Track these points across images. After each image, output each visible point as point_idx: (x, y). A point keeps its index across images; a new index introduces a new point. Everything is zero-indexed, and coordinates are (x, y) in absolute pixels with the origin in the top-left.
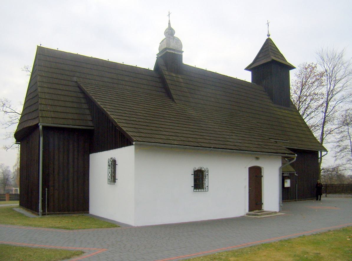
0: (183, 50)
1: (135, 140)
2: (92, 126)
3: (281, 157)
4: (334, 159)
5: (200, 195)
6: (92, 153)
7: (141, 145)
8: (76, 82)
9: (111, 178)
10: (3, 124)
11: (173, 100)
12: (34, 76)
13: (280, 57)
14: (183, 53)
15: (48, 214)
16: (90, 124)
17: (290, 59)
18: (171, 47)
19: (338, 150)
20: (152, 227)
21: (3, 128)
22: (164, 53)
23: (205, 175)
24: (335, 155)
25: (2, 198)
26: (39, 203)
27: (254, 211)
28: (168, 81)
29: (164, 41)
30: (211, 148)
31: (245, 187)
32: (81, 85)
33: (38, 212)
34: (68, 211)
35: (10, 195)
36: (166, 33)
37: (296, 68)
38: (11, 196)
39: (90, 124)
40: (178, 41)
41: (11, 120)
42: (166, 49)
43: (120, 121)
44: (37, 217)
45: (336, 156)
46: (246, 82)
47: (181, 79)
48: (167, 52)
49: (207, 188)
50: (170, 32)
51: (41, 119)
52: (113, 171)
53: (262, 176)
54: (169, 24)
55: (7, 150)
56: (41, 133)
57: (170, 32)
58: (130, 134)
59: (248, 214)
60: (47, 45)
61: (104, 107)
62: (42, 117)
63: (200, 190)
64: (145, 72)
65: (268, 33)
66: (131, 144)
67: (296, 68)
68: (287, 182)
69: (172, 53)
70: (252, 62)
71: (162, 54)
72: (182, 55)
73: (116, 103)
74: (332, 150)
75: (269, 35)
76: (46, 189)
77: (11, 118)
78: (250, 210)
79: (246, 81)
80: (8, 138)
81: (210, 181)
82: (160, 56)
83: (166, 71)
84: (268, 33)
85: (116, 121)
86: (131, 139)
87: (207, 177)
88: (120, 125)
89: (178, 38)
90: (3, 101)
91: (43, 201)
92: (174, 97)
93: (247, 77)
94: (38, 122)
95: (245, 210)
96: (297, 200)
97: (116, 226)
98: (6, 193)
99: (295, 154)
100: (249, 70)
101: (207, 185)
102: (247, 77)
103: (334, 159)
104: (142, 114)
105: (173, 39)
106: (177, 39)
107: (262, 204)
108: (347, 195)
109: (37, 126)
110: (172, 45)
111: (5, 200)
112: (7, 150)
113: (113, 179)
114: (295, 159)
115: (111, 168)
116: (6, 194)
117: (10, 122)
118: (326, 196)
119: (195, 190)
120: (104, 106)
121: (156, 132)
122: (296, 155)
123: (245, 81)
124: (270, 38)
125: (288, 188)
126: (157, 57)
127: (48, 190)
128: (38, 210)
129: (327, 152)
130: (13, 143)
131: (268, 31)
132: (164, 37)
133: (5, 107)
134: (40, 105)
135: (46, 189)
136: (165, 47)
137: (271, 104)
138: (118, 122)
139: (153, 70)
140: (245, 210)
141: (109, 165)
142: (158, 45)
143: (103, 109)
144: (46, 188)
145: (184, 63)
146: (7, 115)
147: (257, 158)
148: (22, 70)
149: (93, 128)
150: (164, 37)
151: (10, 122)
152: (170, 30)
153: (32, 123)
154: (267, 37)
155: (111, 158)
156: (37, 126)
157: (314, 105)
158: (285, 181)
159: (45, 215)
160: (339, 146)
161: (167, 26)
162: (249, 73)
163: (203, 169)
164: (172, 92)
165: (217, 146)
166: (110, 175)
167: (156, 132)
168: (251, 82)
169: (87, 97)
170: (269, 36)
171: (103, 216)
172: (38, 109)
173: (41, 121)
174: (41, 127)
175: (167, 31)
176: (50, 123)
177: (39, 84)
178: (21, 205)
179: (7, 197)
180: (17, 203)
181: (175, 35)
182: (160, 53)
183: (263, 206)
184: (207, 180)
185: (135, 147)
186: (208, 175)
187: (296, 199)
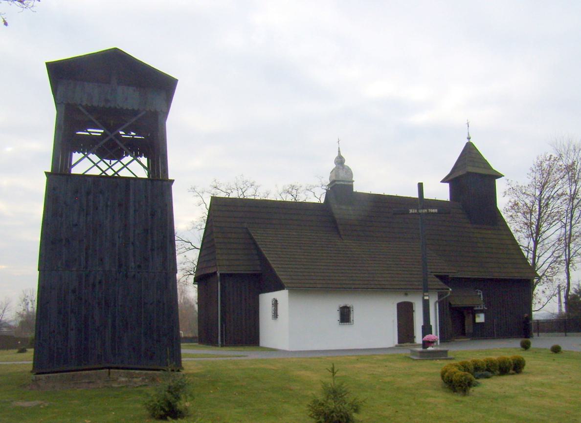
5: (346, 327)
6: (261, 293)
8: (247, 228)
16: (259, 268)
17: (496, 165)
18: (340, 178)
29: (334, 171)
31: (393, 321)
33: (218, 343)
34: (246, 343)
36: (336, 162)
37: (503, 176)
40: (349, 172)
46: (438, 200)
48: (336, 184)
50: (340, 161)
51: (218, 267)
54: (339, 151)
56: (219, 279)
57: (340, 161)
59: (396, 346)
63: (345, 323)
65: (469, 135)
67: (503, 176)
71: (331, 186)
75: (469, 138)
81: (355, 315)
84: (469, 135)
89: (348, 167)
91: (222, 335)
96: (495, 337)
105: (343, 169)
109: (215, 273)
110: (342, 175)
113: (275, 315)
118: (538, 335)
122: (451, 290)
123: (435, 200)
124: (471, 141)
132: (335, 166)
136: (334, 178)
139: (354, 190)
141: (273, 304)
147: (406, 294)
153: (211, 271)
154: (467, 141)
156: (215, 273)
158: (476, 316)
161: (337, 155)
162: (447, 185)
163: (348, 306)
174: (218, 274)
176: (225, 271)
184: (352, 315)
185: (289, 292)
187: (494, 336)
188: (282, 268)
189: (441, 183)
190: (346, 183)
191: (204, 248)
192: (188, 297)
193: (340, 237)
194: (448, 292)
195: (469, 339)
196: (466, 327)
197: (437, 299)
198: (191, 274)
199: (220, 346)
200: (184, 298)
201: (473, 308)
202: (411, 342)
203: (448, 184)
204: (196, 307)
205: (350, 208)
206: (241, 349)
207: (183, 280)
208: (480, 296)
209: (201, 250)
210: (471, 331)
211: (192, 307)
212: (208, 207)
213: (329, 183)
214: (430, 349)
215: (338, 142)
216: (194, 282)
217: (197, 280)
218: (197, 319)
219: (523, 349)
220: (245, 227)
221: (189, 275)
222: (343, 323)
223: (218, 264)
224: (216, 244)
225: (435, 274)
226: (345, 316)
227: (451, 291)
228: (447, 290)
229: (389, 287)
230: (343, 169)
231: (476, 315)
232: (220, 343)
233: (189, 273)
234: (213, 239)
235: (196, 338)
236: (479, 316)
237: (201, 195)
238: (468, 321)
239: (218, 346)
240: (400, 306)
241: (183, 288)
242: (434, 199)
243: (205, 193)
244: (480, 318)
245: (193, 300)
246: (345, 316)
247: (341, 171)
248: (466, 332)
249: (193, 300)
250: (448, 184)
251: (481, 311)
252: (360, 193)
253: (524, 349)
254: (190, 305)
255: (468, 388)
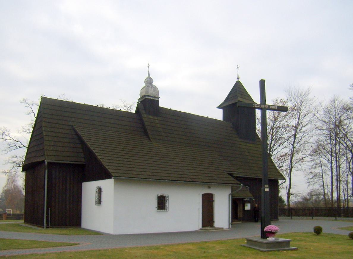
0: (159, 96)
1: (114, 175)
2: (84, 162)
3: (231, 187)
4: (308, 184)
5: (162, 214)
6: (84, 182)
7: (118, 179)
8: (72, 126)
9: (98, 201)
10: (2, 151)
11: (149, 138)
12: (39, 121)
13: (247, 98)
14: (159, 99)
15: (50, 227)
16: (83, 160)
18: (149, 94)
19: (311, 176)
20: (123, 235)
21: (2, 154)
22: (143, 99)
23: (166, 199)
24: (308, 181)
25: (1, 218)
26: (44, 219)
27: (207, 227)
28: (146, 123)
29: (144, 88)
30: (169, 180)
31: (199, 209)
32: (76, 128)
33: (43, 225)
34: (69, 225)
35: (7, 215)
36: (146, 82)
38: (8, 216)
39: (83, 160)
40: (155, 89)
41: (9, 146)
42: (145, 96)
43: (105, 161)
44: (43, 229)
45: (309, 182)
46: (216, 120)
47: (157, 120)
48: (146, 98)
49: (167, 209)
50: (149, 81)
52: (99, 195)
53: (214, 201)
54: (149, 74)
55: (6, 174)
57: (149, 81)
58: (110, 171)
59: (201, 229)
60: (48, 96)
61: (93, 150)
62: (47, 155)
63: (162, 210)
64: (127, 114)
65: (238, 76)
66: (111, 178)
68: (247, 205)
69: (150, 99)
70: (223, 102)
71: (142, 100)
72: (159, 101)
73: (102, 145)
74: (306, 177)
75: (238, 78)
76: (50, 209)
77: (9, 144)
78: (203, 226)
79: (216, 119)
80: (8, 163)
81: (170, 204)
82: (140, 101)
83: (145, 114)
84: (238, 76)
85: (102, 161)
86: (110, 174)
87: (167, 201)
88: (104, 164)
89: (155, 86)
90: (3, 129)
91: (47, 218)
92: (150, 136)
93: (218, 115)
94: (44, 159)
95: (199, 226)
97: (101, 234)
98: (4, 213)
99: (241, 184)
100: (221, 108)
101: (167, 207)
102: (218, 115)
103: (308, 184)
104: (121, 154)
105: (152, 87)
106: (155, 87)
107: (214, 222)
108: (307, 217)
110: (151, 92)
111: (2, 219)
112: (6, 174)
114: (241, 188)
115: (98, 194)
116: (4, 214)
117: (8, 148)
119: (158, 210)
120: (94, 148)
121: (130, 169)
122: (242, 185)
123: (215, 119)
124: (240, 81)
125: (248, 211)
126: (138, 102)
127: (50, 209)
128: (43, 224)
129: (285, 179)
130: (11, 168)
131: (238, 74)
132: (144, 85)
133: (4, 135)
134: (45, 146)
135: (50, 209)
136: (144, 94)
137: (238, 139)
138: (103, 162)
140: (199, 226)
142: (139, 92)
143: (92, 151)
144: (49, 208)
145: (161, 106)
146: (6, 142)
147: (209, 187)
148: (20, 102)
149: (85, 163)
150: (144, 85)
151: (8, 148)
152: (149, 80)
154: (237, 80)
155: (98, 187)
157: (286, 136)
158: (245, 205)
159: (49, 227)
160: (312, 173)
162: (221, 111)
163: (164, 195)
164: (149, 132)
165: (174, 179)
166: (97, 198)
167: (130, 169)
168: (222, 120)
169: (80, 138)
170: (239, 79)
171: (92, 229)
172: (44, 149)
173: (46, 159)
174: (46, 163)
175: (147, 81)
177: (44, 129)
178: (26, 222)
179: (4, 217)
180: (22, 222)
181: (153, 84)
182: (141, 98)
183: (214, 224)
184: (167, 203)
185: (114, 180)
186: (168, 199)
188: (139, 144)
189: (217, 109)
190: (153, 99)
191: (30, 147)
192: (17, 185)
193: (150, 140)
194: (240, 186)
195: (240, 222)
196: (239, 213)
197: (230, 192)
198: (20, 166)
199: (45, 227)
200: (14, 186)
201: (242, 199)
202: (210, 226)
203: (222, 110)
204: (24, 192)
205: (156, 118)
206: (64, 231)
207: (14, 171)
208: (248, 190)
209: (29, 148)
210: (241, 216)
211: (20, 191)
212: (36, 115)
213: (140, 98)
214: (271, 239)
215: (149, 66)
216: (22, 170)
217: (25, 168)
218: (24, 201)
219: (315, 234)
220: (71, 125)
221: (18, 167)
222: (160, 210)
223: (46, 154)
224: (44, 137)
225: (227, 172)
226: (162, 203)
227: (242, 186)
228: (239, 185)
229: (198, 180)
230: (152, 87)
231: (246, 204)
232: (45, 224)
233: (18, 166)
234: (42, 133)
235: (22, 215)
236: (247, 205)
237: (31, 106)
238: (240, 208)
239: (44, 227)
240: (204, 196)
241: (14, 178)
242: (215, 118)
243: (34, 105)
244: (248, 207)
245: (21, 186)
246: (162, 203)
247: (150, 89)
248: (238, 217)
249: (21, 186)
250: (222, 110)
251: (248, 202)
252: (163, 108)
253: (316, 234)
254: (19, 190)
255: (10, 189)
